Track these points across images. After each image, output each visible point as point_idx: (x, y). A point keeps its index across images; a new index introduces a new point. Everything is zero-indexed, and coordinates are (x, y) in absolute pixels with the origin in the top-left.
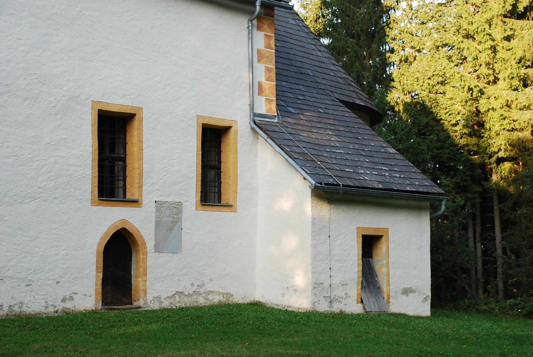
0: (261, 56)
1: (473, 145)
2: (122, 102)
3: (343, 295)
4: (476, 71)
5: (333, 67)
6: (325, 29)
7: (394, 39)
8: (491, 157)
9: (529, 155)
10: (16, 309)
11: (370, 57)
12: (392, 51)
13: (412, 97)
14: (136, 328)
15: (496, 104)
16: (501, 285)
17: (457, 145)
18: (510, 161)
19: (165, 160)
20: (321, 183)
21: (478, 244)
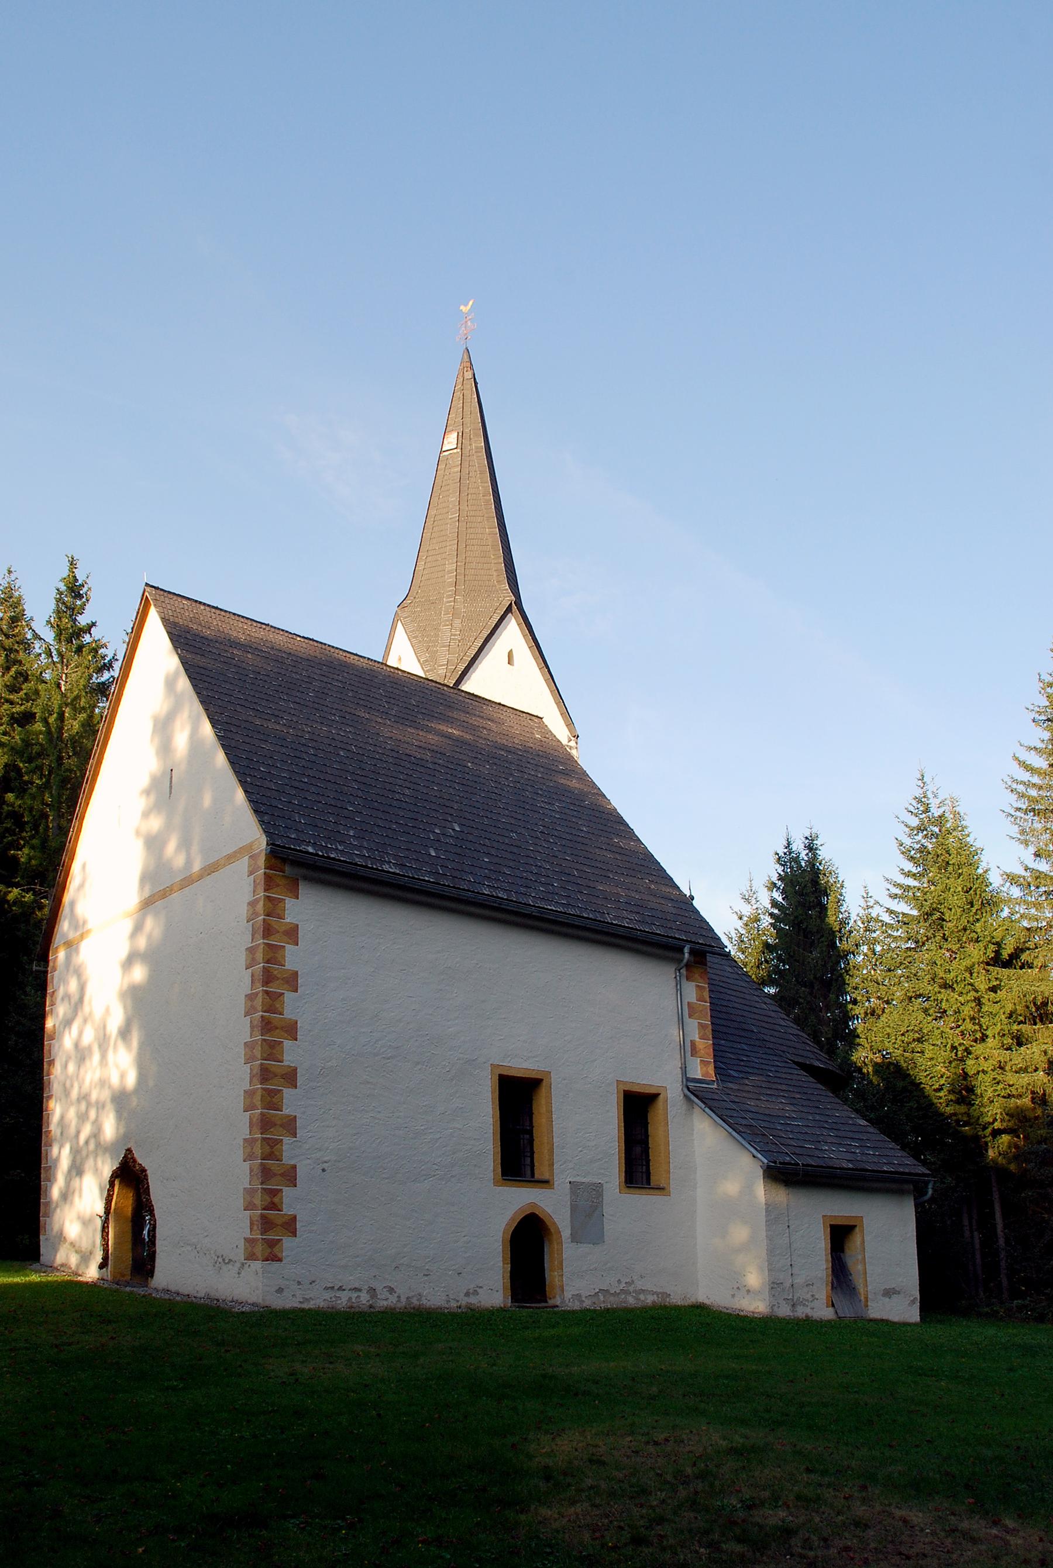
0: (692, 1011)
1: (962, 1114)
2: (525, 1065)
3: (809, 1296)
4: (959, 1026)
5: (782, 1023)
6: (769, 976)
7: (856, 988)
8: (985, 1128)
9: (1031, 1127)
10: (415, 1301)
11: (828, 1008)
12: (855, 1002)
13: (883, 1056)
14: (553, 1332)
15: (987, 1066)
16: (1005, 1282)
17: (942, 1114)
18: (1008, 1133)
19: (581, 1134)
20: (775, 1162)
21: (976, 1233)
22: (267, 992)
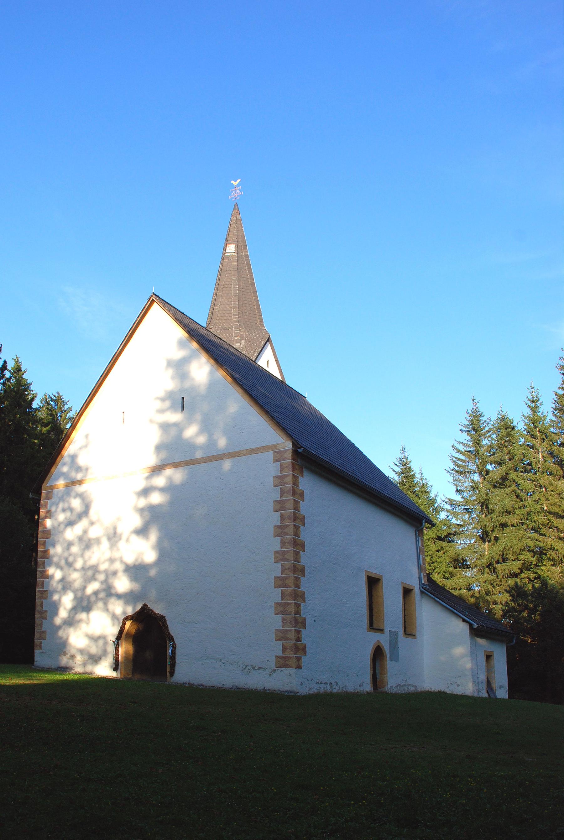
2: (375, 572)
22: (295, 525)
